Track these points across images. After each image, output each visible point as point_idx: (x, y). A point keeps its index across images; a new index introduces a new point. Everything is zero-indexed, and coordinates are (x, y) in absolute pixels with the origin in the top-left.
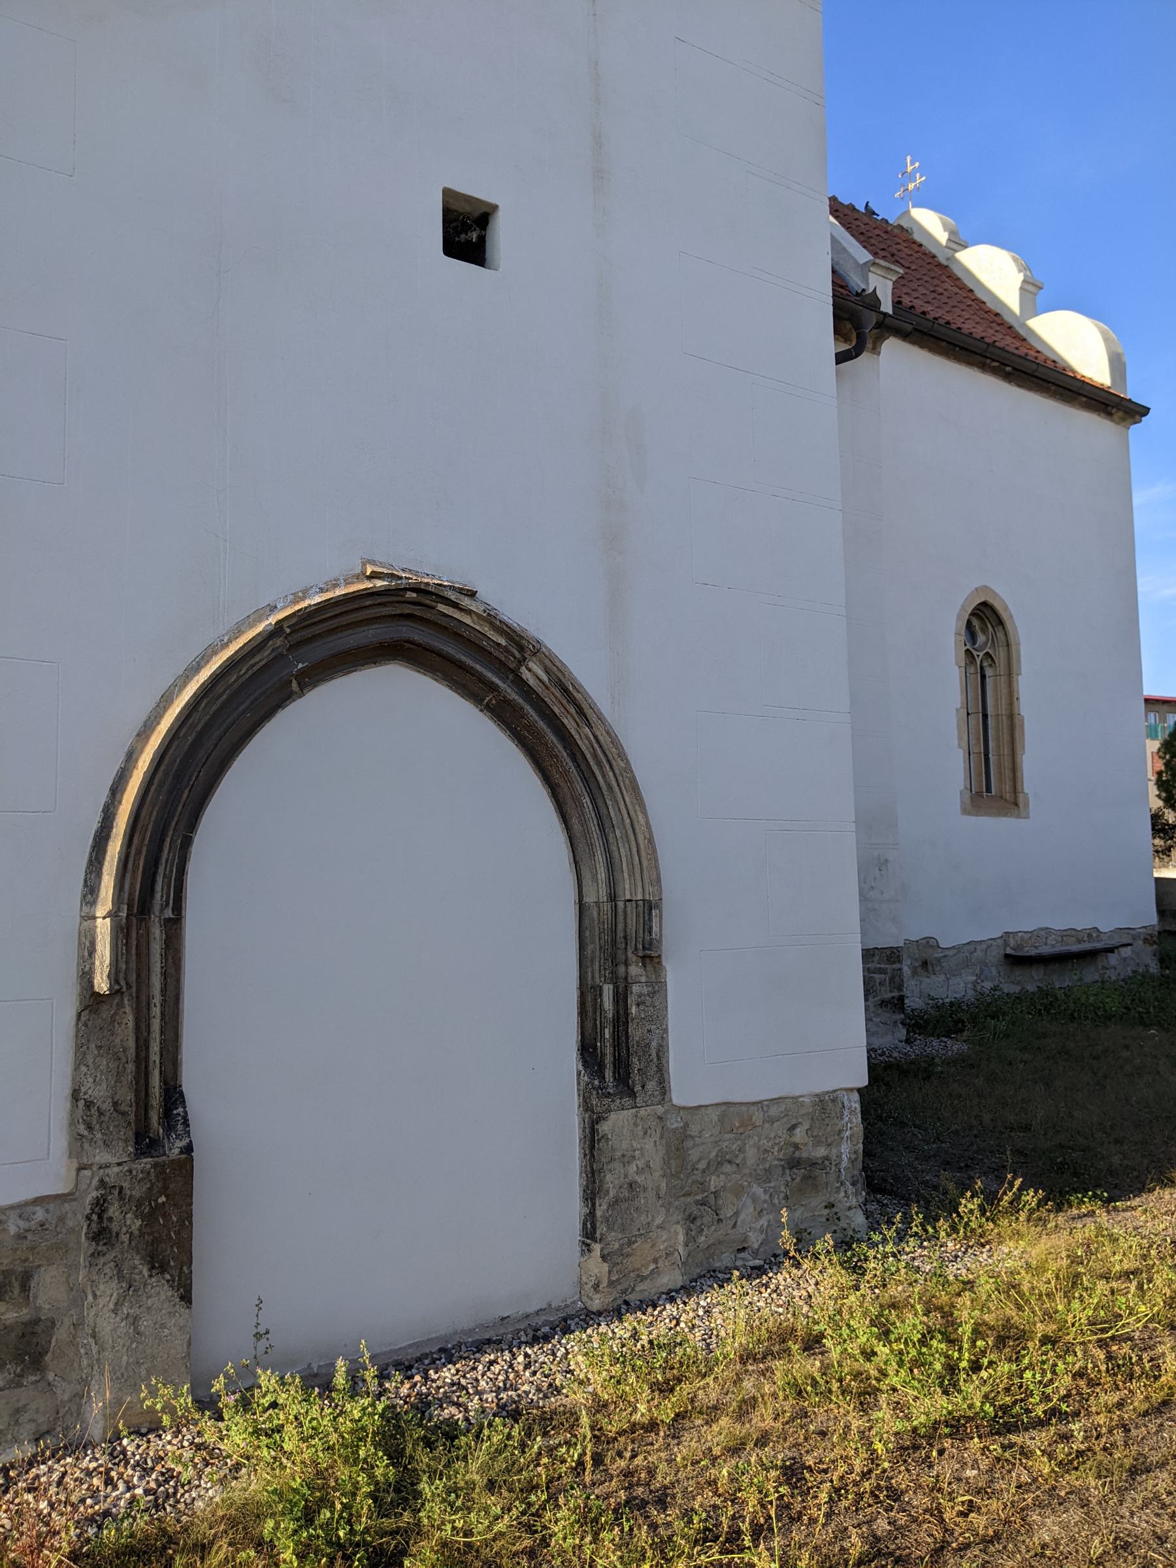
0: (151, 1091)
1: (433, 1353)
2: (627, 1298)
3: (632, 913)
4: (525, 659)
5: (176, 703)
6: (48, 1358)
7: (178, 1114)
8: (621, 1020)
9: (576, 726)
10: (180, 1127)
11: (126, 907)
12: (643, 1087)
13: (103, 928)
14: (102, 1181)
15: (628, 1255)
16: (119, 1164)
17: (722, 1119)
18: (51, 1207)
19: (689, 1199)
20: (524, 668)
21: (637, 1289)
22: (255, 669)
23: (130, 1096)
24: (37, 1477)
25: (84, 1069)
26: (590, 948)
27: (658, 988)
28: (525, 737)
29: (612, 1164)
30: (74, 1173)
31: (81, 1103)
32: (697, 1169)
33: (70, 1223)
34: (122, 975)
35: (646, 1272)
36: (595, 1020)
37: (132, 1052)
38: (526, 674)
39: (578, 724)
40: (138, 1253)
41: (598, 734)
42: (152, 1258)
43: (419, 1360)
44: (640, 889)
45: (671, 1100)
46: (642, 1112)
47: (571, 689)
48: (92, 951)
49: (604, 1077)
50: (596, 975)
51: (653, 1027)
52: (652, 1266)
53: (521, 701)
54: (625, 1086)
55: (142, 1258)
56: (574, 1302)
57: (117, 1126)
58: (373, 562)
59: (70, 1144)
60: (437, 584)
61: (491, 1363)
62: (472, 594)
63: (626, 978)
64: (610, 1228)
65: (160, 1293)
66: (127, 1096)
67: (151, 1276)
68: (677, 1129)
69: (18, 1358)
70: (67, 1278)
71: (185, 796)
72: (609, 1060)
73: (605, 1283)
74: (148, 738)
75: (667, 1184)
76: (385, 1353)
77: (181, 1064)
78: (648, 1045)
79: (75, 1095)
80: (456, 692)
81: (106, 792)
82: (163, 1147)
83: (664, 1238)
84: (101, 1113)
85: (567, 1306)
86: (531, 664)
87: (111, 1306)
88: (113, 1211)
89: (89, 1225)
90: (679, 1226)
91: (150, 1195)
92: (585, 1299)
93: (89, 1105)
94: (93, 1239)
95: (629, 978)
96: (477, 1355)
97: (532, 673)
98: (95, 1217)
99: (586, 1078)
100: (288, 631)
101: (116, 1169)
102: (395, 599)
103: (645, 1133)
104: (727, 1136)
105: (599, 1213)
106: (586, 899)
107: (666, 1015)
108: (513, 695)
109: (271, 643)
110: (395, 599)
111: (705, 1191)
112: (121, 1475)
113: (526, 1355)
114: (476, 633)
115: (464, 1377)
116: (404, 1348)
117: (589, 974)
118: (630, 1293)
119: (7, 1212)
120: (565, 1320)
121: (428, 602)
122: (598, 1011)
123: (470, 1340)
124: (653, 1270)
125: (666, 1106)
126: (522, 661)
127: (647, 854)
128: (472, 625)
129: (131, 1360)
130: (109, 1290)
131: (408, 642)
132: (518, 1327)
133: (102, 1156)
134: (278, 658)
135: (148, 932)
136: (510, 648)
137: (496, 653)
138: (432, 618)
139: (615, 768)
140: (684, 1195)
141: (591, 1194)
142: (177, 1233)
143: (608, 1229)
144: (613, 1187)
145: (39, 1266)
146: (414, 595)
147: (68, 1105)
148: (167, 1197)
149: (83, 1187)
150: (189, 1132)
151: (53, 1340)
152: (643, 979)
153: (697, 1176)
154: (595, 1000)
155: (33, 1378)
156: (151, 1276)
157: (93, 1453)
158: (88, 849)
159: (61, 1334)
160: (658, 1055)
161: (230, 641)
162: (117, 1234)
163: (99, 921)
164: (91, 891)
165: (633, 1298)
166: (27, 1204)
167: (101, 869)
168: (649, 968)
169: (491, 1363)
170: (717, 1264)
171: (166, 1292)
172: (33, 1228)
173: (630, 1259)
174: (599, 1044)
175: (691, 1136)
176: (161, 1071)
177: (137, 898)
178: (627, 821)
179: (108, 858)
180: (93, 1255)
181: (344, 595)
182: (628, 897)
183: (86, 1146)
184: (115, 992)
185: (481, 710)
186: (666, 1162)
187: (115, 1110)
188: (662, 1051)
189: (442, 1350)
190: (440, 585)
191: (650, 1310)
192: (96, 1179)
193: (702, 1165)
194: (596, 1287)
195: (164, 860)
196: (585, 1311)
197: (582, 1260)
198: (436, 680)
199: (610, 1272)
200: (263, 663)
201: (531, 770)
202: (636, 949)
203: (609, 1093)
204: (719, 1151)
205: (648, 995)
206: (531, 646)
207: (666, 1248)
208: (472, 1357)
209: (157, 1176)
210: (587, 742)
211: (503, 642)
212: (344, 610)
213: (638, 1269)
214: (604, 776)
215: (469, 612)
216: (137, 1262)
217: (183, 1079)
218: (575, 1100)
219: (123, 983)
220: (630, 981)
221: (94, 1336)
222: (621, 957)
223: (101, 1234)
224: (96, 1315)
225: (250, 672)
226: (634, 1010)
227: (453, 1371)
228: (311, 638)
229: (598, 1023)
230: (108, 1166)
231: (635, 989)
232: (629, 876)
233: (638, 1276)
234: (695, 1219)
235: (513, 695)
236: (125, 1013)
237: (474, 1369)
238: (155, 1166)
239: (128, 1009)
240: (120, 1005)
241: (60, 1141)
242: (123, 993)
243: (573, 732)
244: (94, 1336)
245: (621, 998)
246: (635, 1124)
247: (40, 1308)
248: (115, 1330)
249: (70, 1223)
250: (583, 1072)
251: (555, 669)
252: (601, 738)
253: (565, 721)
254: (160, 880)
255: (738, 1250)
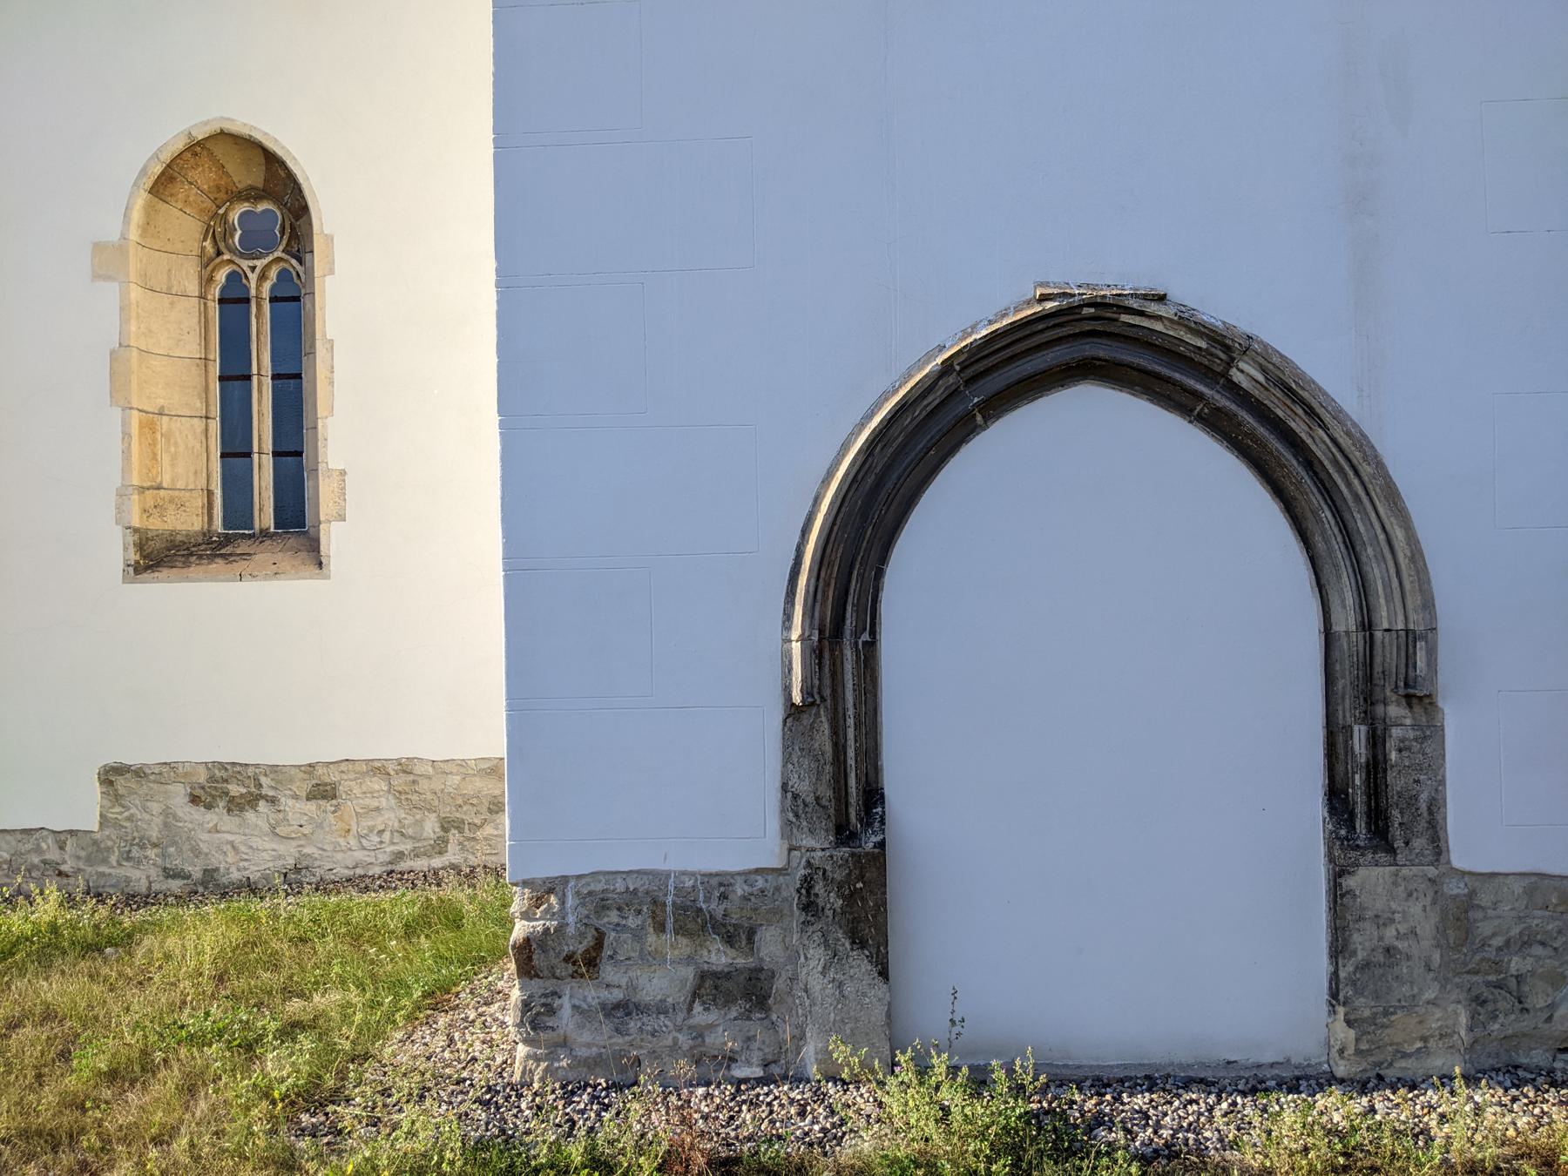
0: (850, 790)
1: (1137, 1078)
2: (1382, 1072)
3: (1391, 645)
4: (1233, 359)
5: (852, 450)
6: (771, 1001)
7: (877, 813)
8: (1376, 767)
9: (1307, 429)
10: (877, 824)
11: (817, 632)
12: (1407, 843)
13: (796, 647)
14: (808, 862)
15: (1383, 1026)
16: (823, 850)
17: (1530, 892)
18: (770, 877)
19: (1475, 978)
20: (1234, 370)
21: (1397, 1065)
22: (929, 409)
23: (829, 793)
24: (758, 1095)
25: (790, 766)
26: (1340, 684)
27: (1431, 731)
28: (1249, 447)
29: (1361, 923)
30: (786, 853)
31: (789, 795)
32: (1489, 946)
33: (785, 894)
34: (815, 690)
35: (1409, 1049)
36: (1347, 764)
37: (829, 755)
38: (1236, 376)
39: (1310, 427)
40: (841, 927)
41: (1336, 435)
42: (853, 934)
43: (1121, 1081)
44: (1401, 617)
45: (1449, 862)
46: (1405, 871)
47: (1294, 387)
48: (790, 670)
49: (1354, 828)
50: (1347, 711)
51: (1422, 777)
52: (1419, 1045)
53: (1233, 407)
54: (1382, 838)
55: (844, 933)
56: (1320, 1064)
57: (819, 818)
58: (1042, 285)
59: (782, 828)
60: (1116, 295)
61: (1191, 1102)
62: (1161, 298)
63: (1384, 720)
64: (1359, 992)
65: (860, 966)
66: (826, 793)
67: (852, 950)
68: (1457, 896)
69: (747, 996)
70: (783, 941)
71: (869, 533)
72: (1360, 809)
73: (1350, 1050)
74: (829, 484)
75: (1442, 956)
76: (1091, 1067)
77: (882, 769)
78: (1416, 798)
79: (785, 787)
80: (1159, 405)
81: (799, 533)
82: (860, 840)
83: (1437, 1016)
84: (806, 805)
85: (1309, 1065)
86: (1242, 365)
87: (820, 969)
88: (819, 888)
89: (799, 898)
90: (1459, 1006)
91: (848, 879)
92: (1332, 1063)
93: (795, 797)
94: (803, 909)
95: (1387, 720)
96: (1180, 1091)
97: (1245, 374)
98: (803, 891)
99: (1330, 826)
100: (958, 368)
101: (820, 854)
102: (1071, 318)
103: (1410, 895)
104: (1540, 913)
105: (1342, 974)
106: (1335, 628)
107: (1443, 765)
108: (1223, 402)
109: (941, 382)
110: (1071, 318)
111: (1501, 972)
112: (813, 1110)
113: (1234, 1104)
114: (1170, 339)
115: (1155, 1108)
116: (1112, 1067)
117: (1341, 713)
118: (1387, 1068)
119: (736, 877)
120: (1298, 1079)
121: (1109, 315)
122: (1350, 753)
123: (1182, 1074)
124: (1421, 1048)
125: (1442, 869)
126: (1230, 363)
127: (1410, 575)
128: (1165, 331)
129: (837, 1018)
130: (817, 956)
131: (1093, 359)
132: (1242, 1074)
133: (808, 842)
134: (953, 394)
135: (841, 651)
136: (1213, 350)
137: (1197, 358)
138: (1117, 331)
139: (1363, 474)
140: (1468, 972)
141: (1339, 949)
142: (874, 917)
143: (1356, 992)
144: (1363, 949)
145: (761, 925)
146: (1092, 310)
147: (779, 795)
148: (864, 883)
149: (794, 864)
150: (884, 830)
151: (774, 987)
152: (1408, 722)
153: (1491, 953)
154: (1347, 741)
155: (759, 1016)
156: (852, 950)
157: (804, 1088)
158: (786, 583)
159: (780, 984)
160: (1429, 809)
161: (900, 387)
162: (823, 909)
163: (794, 643)
164: (788, 617)
165: (1390, 1074)
166: (751, 872)
167: (794, 599)
168: (1417, 709)
169: (1191, 1102)
170: (1523, 1060)
171: (866, 966)
172: (755, 893)
173: (1388, 1031)
174: (1350, 790)
175: (1479, 907)
176: (857, 774)
177: (828, 625)
178: (1382, 537)
179: (798, 591)
180: (803, 923)
181: (1011, 324)
182: (1386, 626)
183: (795, 830)
184: (808, 705)
185: (1190, 422)
186: (1441, 931)
187: (817, 803)
188: (1436, 806)
189: (1147, 1077)
190: (1119, 295)
191: (1402, 1091)
192: (804, 860)
193: (1498, 942)
194: (1341, 1051)
195: (852, 591)
196: (1328, 1076)
197: (1330, 1020)
198: (1133, 395)
199: (1357, 1040)
200: (937, 402)
201: (1258, 483)
202: (1396, 687)
203: (1358, 846)
204: (1525, 929)
205: (1416, 739)
206: (1237, 345)
207: (1440, 1028)
208: (1175, 1091)
209: (854, 864)
210: (1324, 447)
211: (1203, 344)
212: (1014, 338)
213: (1397, 1044)
214: (1349, 485)
215: (1159, 318)
216: (840, 936)
217: (885, 782)
218: (1322, 849)
219: (817, 697)
220: (1389, 723)
221: (806, 991)
222: (1378, 694)
223: (810, 907)
224: (808, 974)
225: (924, 413)
226: (1393, 756)
227: (1146, 1100)
228: (984, 371)
229: (1349, 767)
230: (813, 850)
231: (1396, 732)
232: (1387, 601)
233: (1397, 1051)
234: (1485, 1002)
235: (1223, 402)
236: (821, 722)
237: (1171, 1103)
238: (853, 855)
239: (824, 719)
240: (818, 715)
241: (774, 824)
242: (819, 705)
243: (1303, 435)
244: (806, 991)
245: (1376, 741)
246: (1395, 884)
247: (762, 960)
248: (824, 989)
249: (785, 894)
250: (1328, 819)
251: (1271, 367)
252: (1341, 440)
253: (1293, 425)
254: (849, 608)
255: (1559, 1049)
